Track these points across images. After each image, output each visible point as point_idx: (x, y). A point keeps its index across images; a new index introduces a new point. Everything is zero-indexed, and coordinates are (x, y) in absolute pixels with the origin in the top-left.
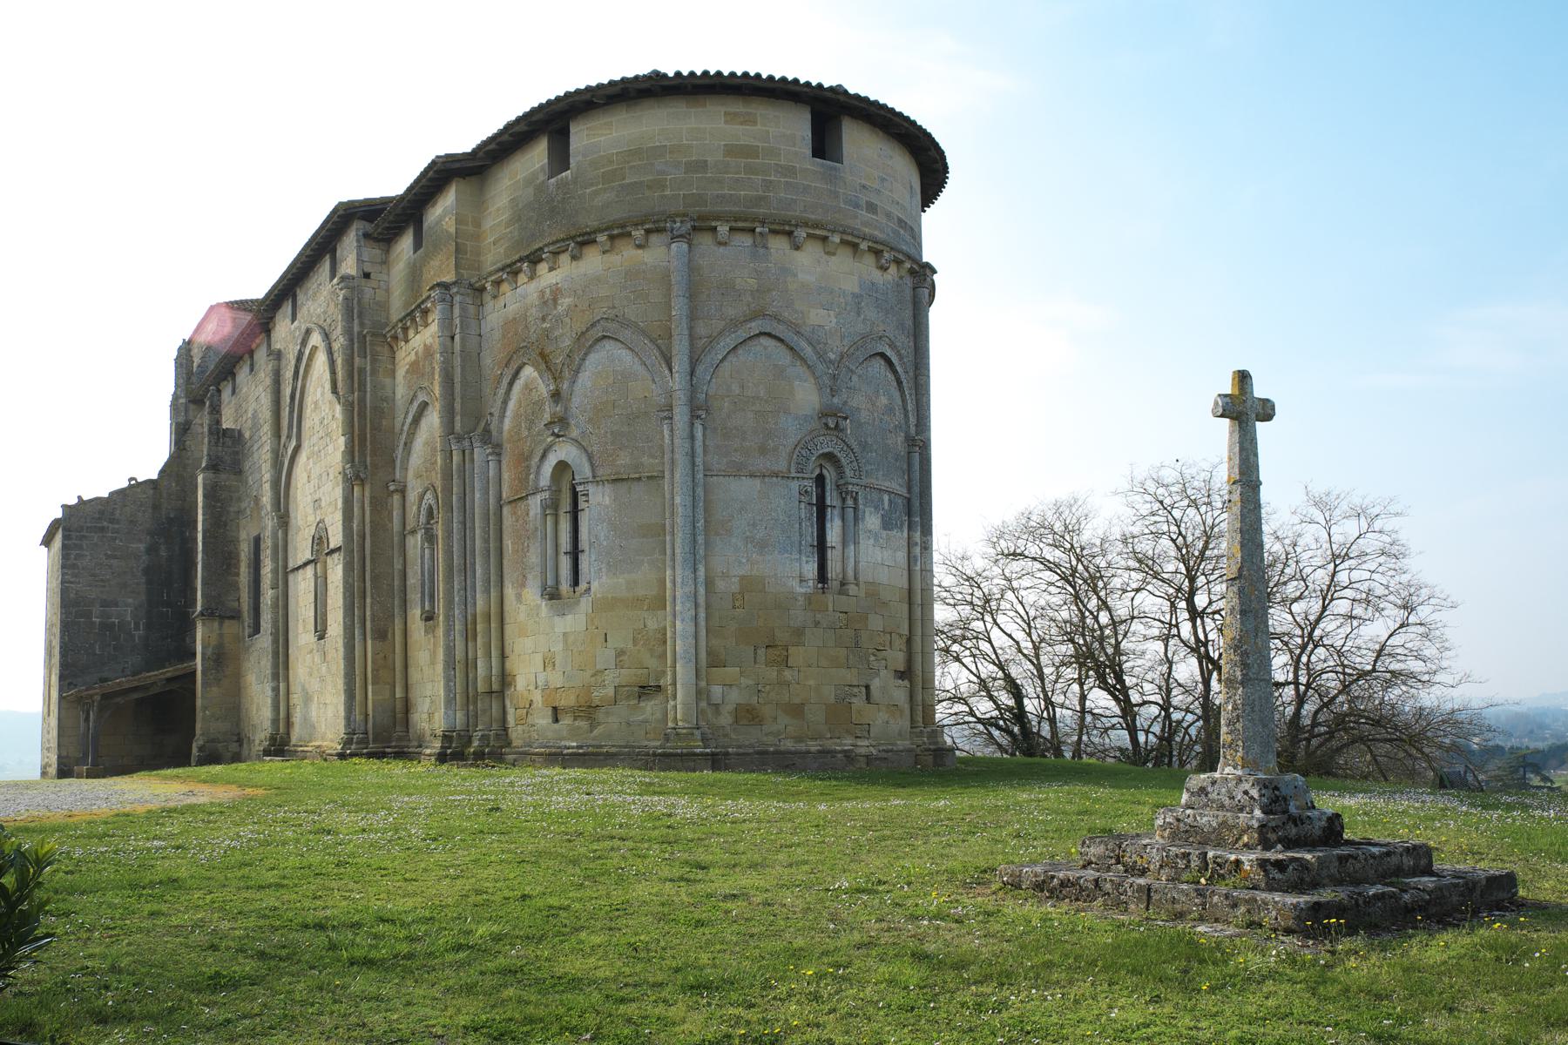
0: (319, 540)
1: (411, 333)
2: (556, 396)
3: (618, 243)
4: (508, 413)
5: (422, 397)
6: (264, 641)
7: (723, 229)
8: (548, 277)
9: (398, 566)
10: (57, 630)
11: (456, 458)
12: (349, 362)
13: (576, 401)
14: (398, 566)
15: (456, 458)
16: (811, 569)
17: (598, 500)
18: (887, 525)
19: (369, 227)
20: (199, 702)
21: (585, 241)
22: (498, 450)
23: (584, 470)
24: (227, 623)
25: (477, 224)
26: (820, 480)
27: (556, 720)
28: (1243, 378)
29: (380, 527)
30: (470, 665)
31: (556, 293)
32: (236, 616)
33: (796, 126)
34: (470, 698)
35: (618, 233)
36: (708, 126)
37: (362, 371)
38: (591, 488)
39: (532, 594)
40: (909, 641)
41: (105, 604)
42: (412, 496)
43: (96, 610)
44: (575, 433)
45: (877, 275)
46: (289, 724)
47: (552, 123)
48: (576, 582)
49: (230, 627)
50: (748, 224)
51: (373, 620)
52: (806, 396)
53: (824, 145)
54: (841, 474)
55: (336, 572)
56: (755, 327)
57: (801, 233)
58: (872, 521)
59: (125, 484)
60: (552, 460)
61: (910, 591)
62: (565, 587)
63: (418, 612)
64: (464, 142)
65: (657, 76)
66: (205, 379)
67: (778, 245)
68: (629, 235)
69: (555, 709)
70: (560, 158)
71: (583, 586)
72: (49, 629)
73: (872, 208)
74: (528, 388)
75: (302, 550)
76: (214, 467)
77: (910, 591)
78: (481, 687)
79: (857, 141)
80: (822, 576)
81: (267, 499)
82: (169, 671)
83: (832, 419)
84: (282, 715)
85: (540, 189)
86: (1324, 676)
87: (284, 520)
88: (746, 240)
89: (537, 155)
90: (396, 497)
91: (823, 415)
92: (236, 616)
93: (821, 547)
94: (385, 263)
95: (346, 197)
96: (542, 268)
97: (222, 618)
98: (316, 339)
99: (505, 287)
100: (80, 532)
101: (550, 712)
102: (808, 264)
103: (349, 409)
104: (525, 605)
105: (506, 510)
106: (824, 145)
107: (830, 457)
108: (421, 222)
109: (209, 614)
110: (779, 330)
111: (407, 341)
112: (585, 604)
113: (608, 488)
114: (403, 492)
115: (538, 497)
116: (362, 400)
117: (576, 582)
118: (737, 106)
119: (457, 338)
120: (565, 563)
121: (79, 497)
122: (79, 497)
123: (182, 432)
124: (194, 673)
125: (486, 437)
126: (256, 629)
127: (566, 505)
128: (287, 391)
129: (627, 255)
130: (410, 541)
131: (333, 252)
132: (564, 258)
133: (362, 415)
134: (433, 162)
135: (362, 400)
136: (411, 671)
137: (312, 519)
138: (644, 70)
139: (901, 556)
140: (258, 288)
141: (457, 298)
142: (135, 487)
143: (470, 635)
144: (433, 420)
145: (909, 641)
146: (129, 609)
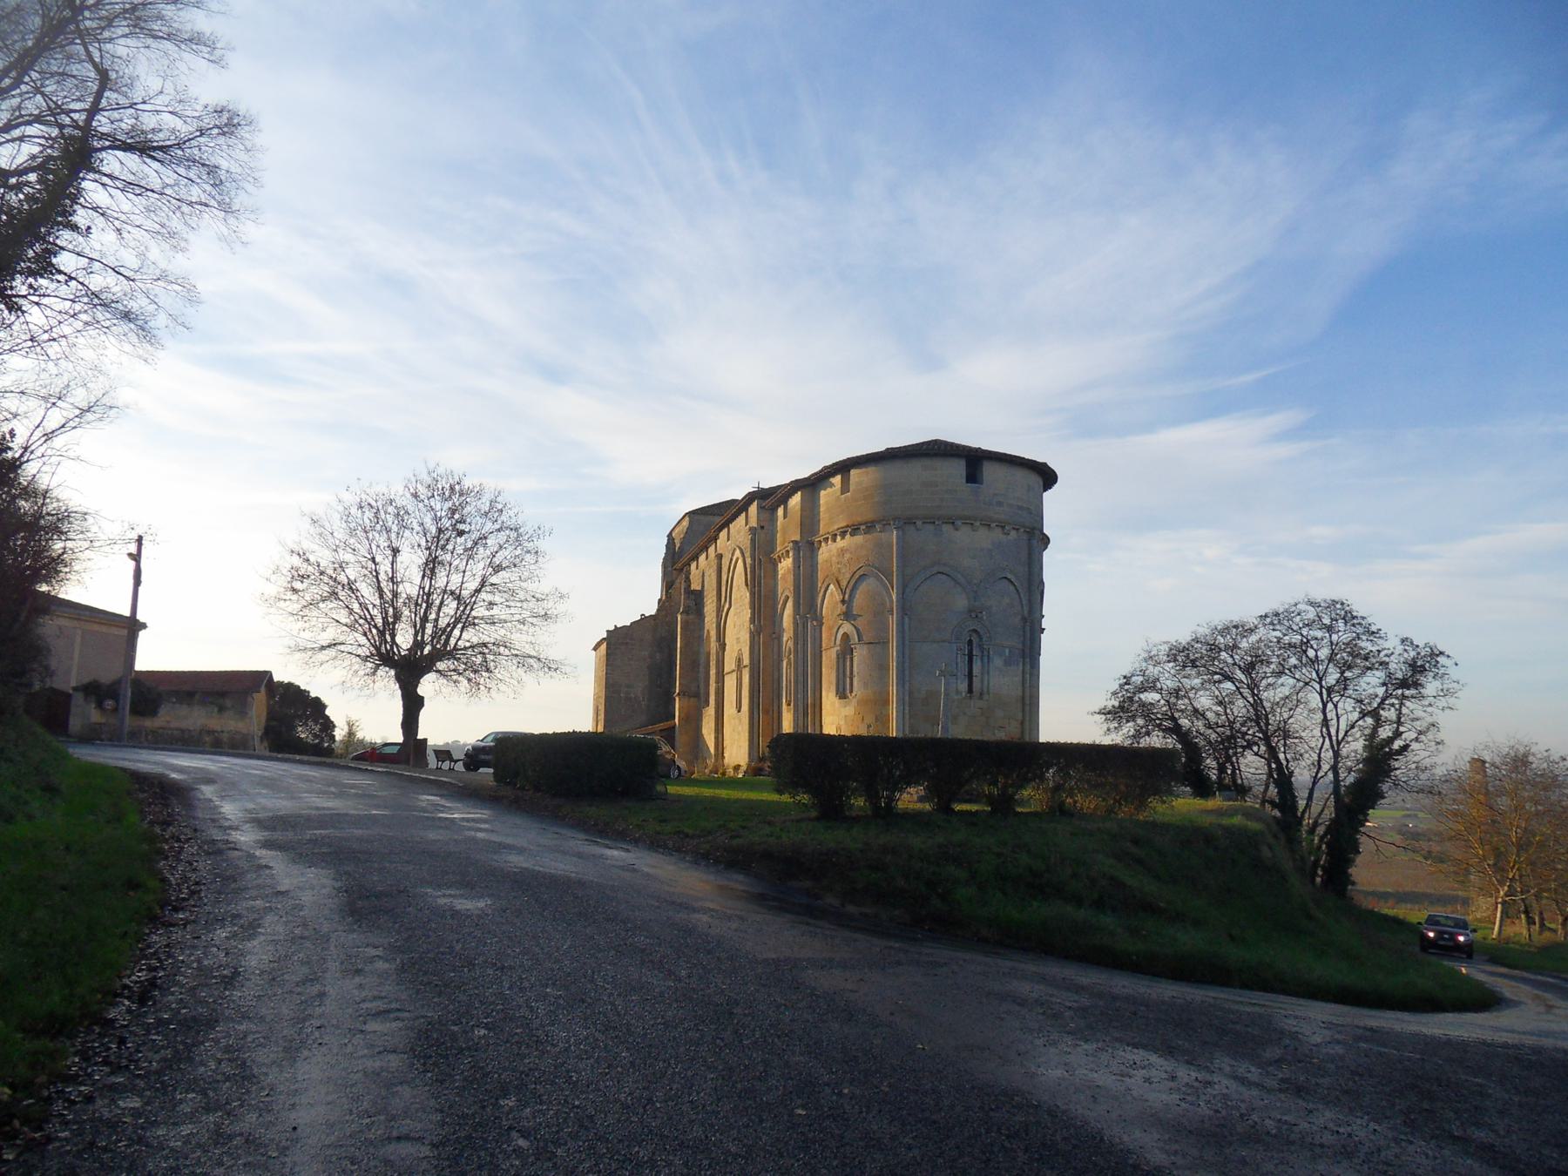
0: (739, 660)
7: (919, 523)
10: (602, 701)
12: (753, 572)
16: (963, 686)
18: (1007, 663)
26: (970, 642)
33: (958, 468)
36: (915, 472)
40: (1022, 723)
41: (628, 686)
45: (1002, 537)
50: (930, 520)
52: (961, 602)
53: (973, 477)
54: (981, 638)
56: (935, 570)
57: (959, 523)
58: (998, 662)
61: (1023, 698)
66: (677, 560)
67: (946, 528)
72: (596, 699)
73: (1000, 504)
75: (729, 665)
77: (1023, 698)
79: (989, 471)
80: (970, 690)
81: (713, 633)
83: (973, 613)
85: (838, 499)
87: (722, 646)
88: (931, 527)
91: (970, 611)
93: (970, 675)
98: (738, 553)
100: (618, 643)
102: (963, 537)
103: (752, 594)
104: (829, 699)
106: (973, 477)
107: (975, 631)
109: (682, 694)
110: (946, 570)
118: (927, 462)
123: (668, 584)
128: (724, 577)
137: (736, 648)
139: (1018, 679)
142: (644, 619)
144: (790, 604)
145: (1022, 723)
146: (639, 688)
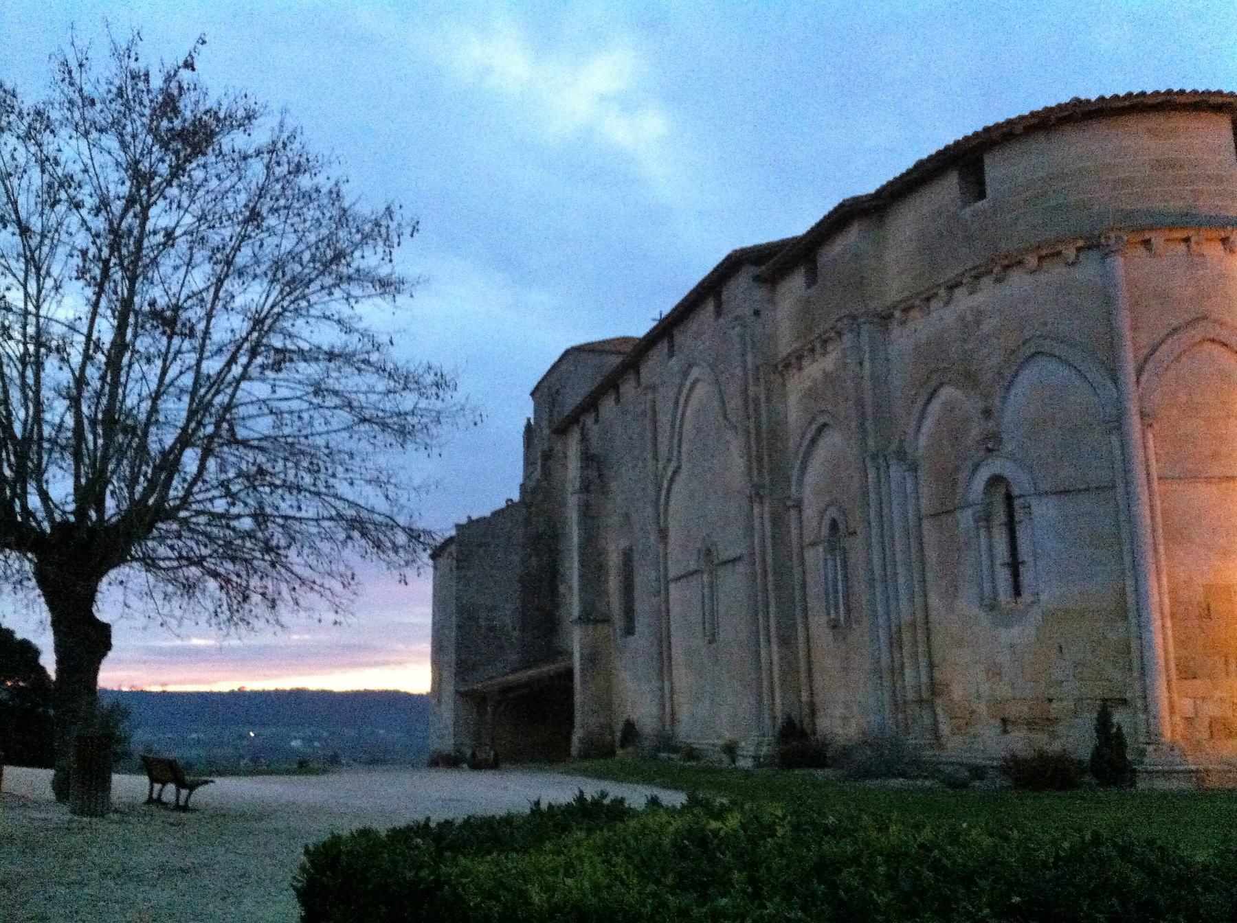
1: (805, 363)
2: (987, 413)
3: (1046, 264)
4: (924, 430)
5: (821, 420)
6: (642, 640)
8: (964, 302)
9: (797, 577)
11: (872, 475)
13: (1008, 418)
14: (797, 577)
15: (872, 475)
17: (1045, 511)
19: (756, 270)
20: (578, 698)
21: (1013, 263)
22: (914, 468)
23: (1021, 482)
24: (600, 626)
25: (879, 258)
27: (1005, 731)
28: (193, 70)
29: (780, 538)
30: (896, 671)
31: (979, 313)
32: (607, 620)
34: (898, 704)
35: (1049, 254)
37: (756, 400)
38: (1034, 502)
39: (967, 604)
42: (810, 512)
43: (483, 615)
44: (1009, 447)
46: (674, 720)
47: (965, 160)
48: (1017, 591)
49: (603, 630)
51: (778, 628)
55: (733, 584)
59: (503, 505)
60: (984, 474)
62: (1004, 596)
63: (823, 619)
64: (869, 186)
65: (1077, 102)
68: (1059, 253)
69: (1004, 721)
70: (976, 187)
71: (1026, 597)
74: (949, 407)
75: (679, 559)
76: (586, 488)
78: (911, 695)
82: (547, 669)
84: (668, 709)
86: (134, 396)
89: (949, 187)
90: (793, 512)
92: (607, 620)
94: (772, 301)
95: (738, 246)
96: (959, 293)
97: (596, 622)
99: (914, 313)
101: (998, 723)
105: (926, 524)
108: (814, 262)
111: (800, 369)
112: (1035, 615)
113: (1052, 501)
114: (799, 506)
115: (970, 511)
116: (758, 427)
117: (1017, 591)
119: (867, 364)
120: (1003, 575)
121: (469, 517)
122: (469, 517)
124: (569, 673)
125: (901, 455)
126: (629, 631)
127: (1000, 516)
129: (1056, 273)
130: (810, 555)
131: (718, 296)
132: (987, 281)
133: (758, 439)
134: (841, 205)
135: (758, 427)
136: (817, 677)
138: (1065, 99)
140: (640, 328)
141: (865, 328)
143: (895, 643)
